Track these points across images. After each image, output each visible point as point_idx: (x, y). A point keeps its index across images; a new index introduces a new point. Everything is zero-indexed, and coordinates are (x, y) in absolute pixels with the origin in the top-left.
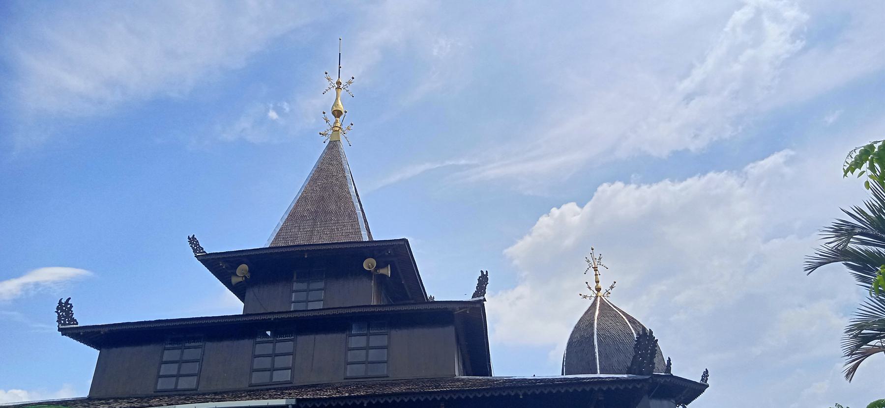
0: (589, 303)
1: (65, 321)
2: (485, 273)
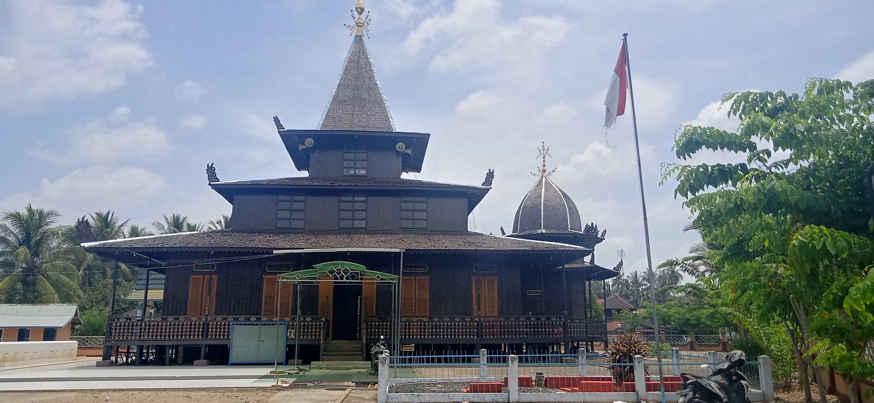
0: (537, 179)
1: (212, 179)
2: (492, 171)
